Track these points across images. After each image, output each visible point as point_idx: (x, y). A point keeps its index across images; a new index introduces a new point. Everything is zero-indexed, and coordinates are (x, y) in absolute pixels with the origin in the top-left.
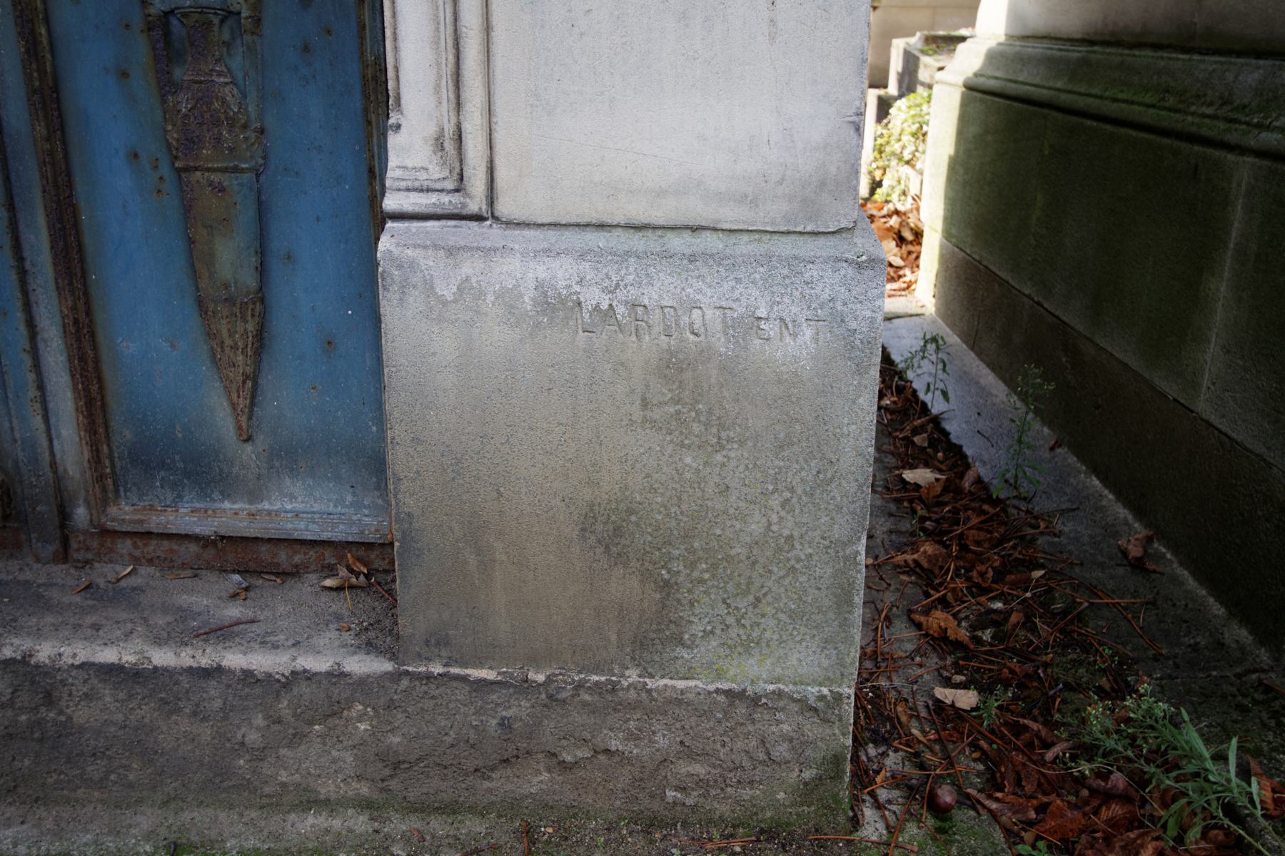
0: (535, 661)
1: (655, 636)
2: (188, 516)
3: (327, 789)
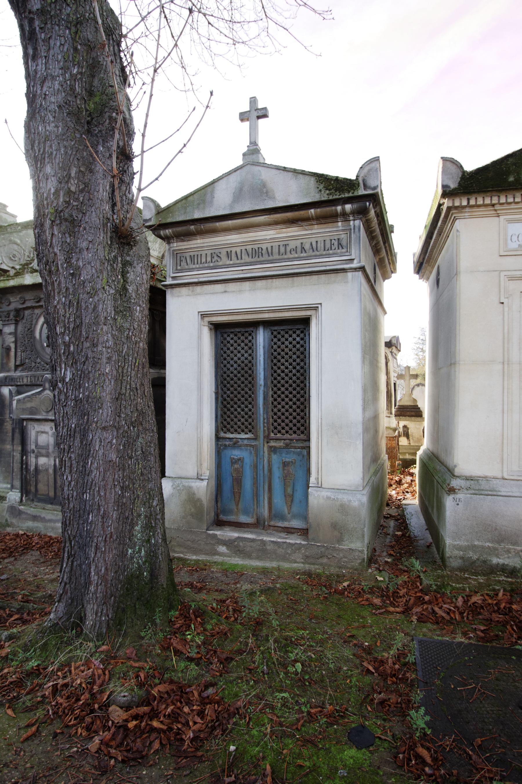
0: (325, 543)
1: (340, 540)
2: (280, 524)
3: (298, 560)
